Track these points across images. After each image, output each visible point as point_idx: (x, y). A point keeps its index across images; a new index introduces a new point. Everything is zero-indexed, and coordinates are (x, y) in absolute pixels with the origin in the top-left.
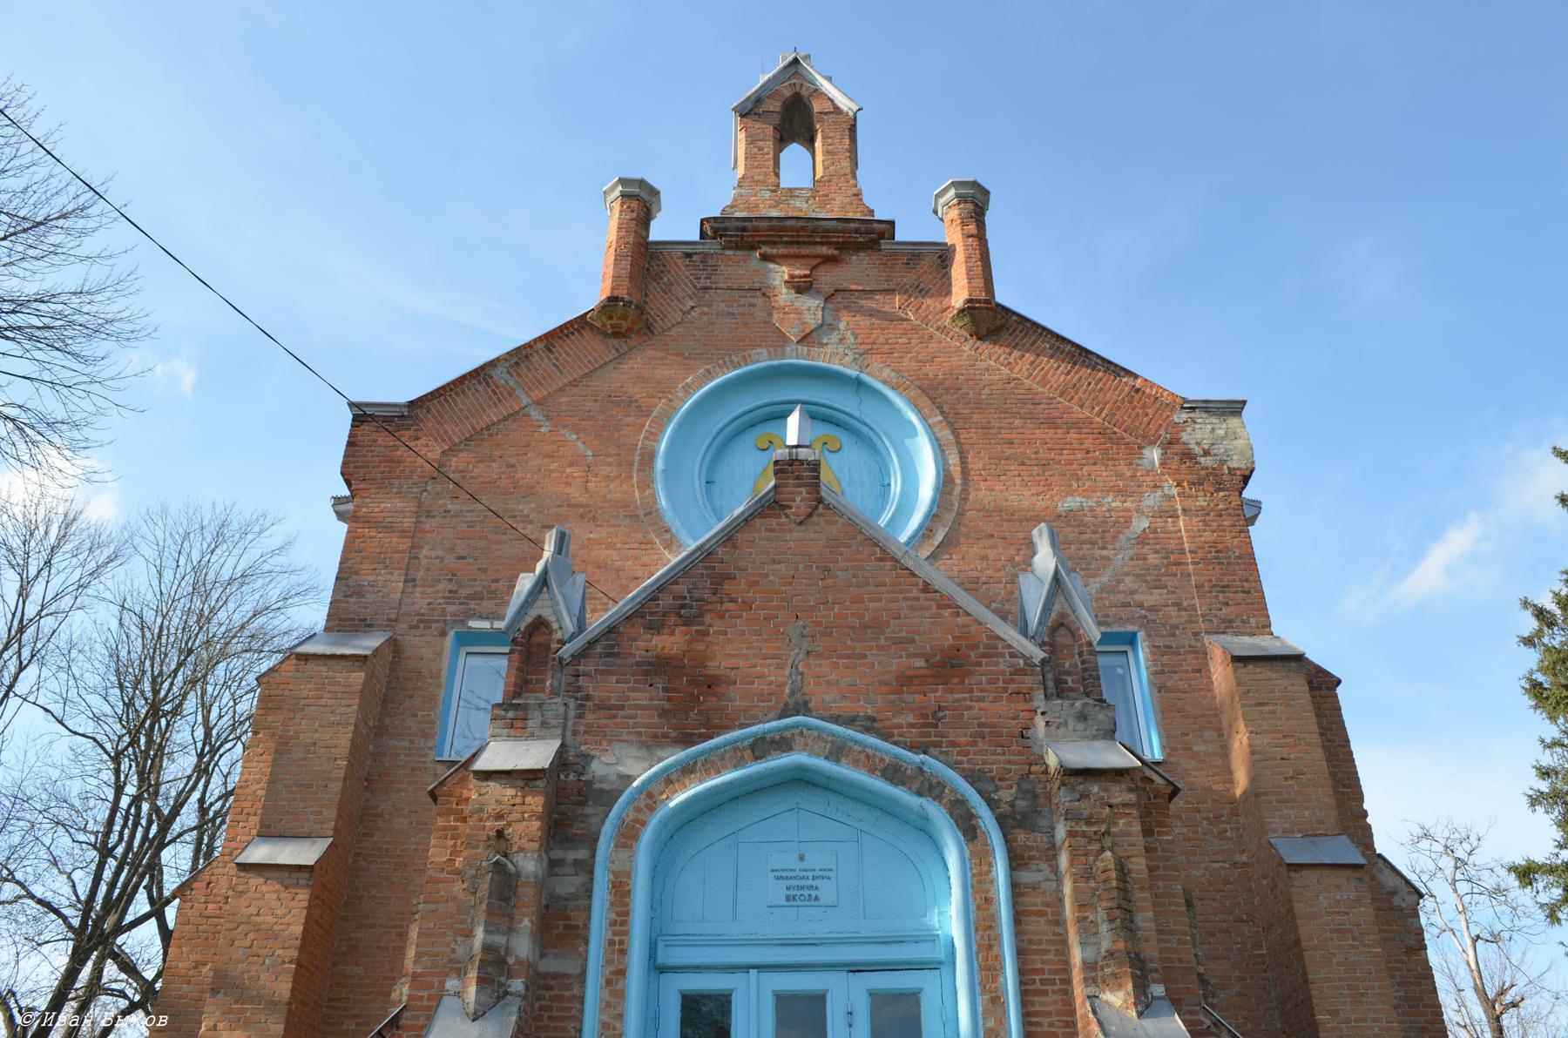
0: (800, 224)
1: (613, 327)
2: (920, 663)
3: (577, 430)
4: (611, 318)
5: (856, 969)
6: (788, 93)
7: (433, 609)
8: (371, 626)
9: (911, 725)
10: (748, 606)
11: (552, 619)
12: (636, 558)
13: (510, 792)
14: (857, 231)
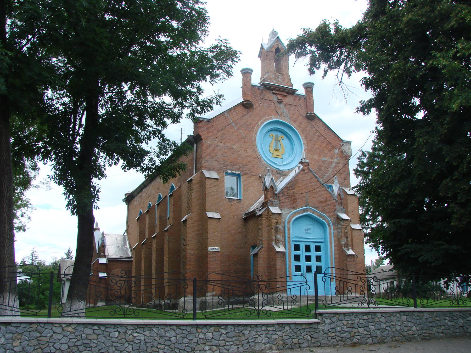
6: (276, 47)
8: (210, 169)
11: (273, 186)
14: (292, 91)
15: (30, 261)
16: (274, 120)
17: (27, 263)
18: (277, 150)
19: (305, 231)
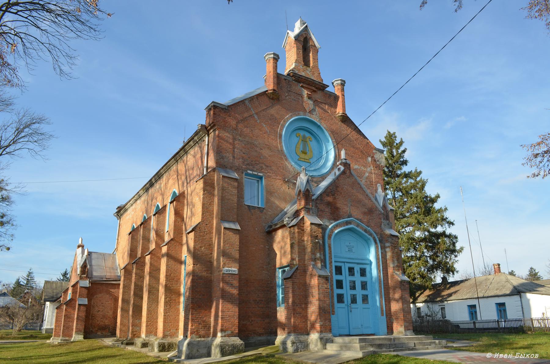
0: (311, 80)
1: (272, 97)
2: (366, 210)
3: (265, 124)
4: (273, 95)
5: (358, 264)
7: (239, 166)
9: (366, 222)
10: (341, 193)
11: (310, 190)
12: (279, 161)
13: (316, 228)
14: (322, 86)
15: (25, 282)
16: (302, 117)
17: (22, 283)
18: (304, 152)
19: (347, 250)
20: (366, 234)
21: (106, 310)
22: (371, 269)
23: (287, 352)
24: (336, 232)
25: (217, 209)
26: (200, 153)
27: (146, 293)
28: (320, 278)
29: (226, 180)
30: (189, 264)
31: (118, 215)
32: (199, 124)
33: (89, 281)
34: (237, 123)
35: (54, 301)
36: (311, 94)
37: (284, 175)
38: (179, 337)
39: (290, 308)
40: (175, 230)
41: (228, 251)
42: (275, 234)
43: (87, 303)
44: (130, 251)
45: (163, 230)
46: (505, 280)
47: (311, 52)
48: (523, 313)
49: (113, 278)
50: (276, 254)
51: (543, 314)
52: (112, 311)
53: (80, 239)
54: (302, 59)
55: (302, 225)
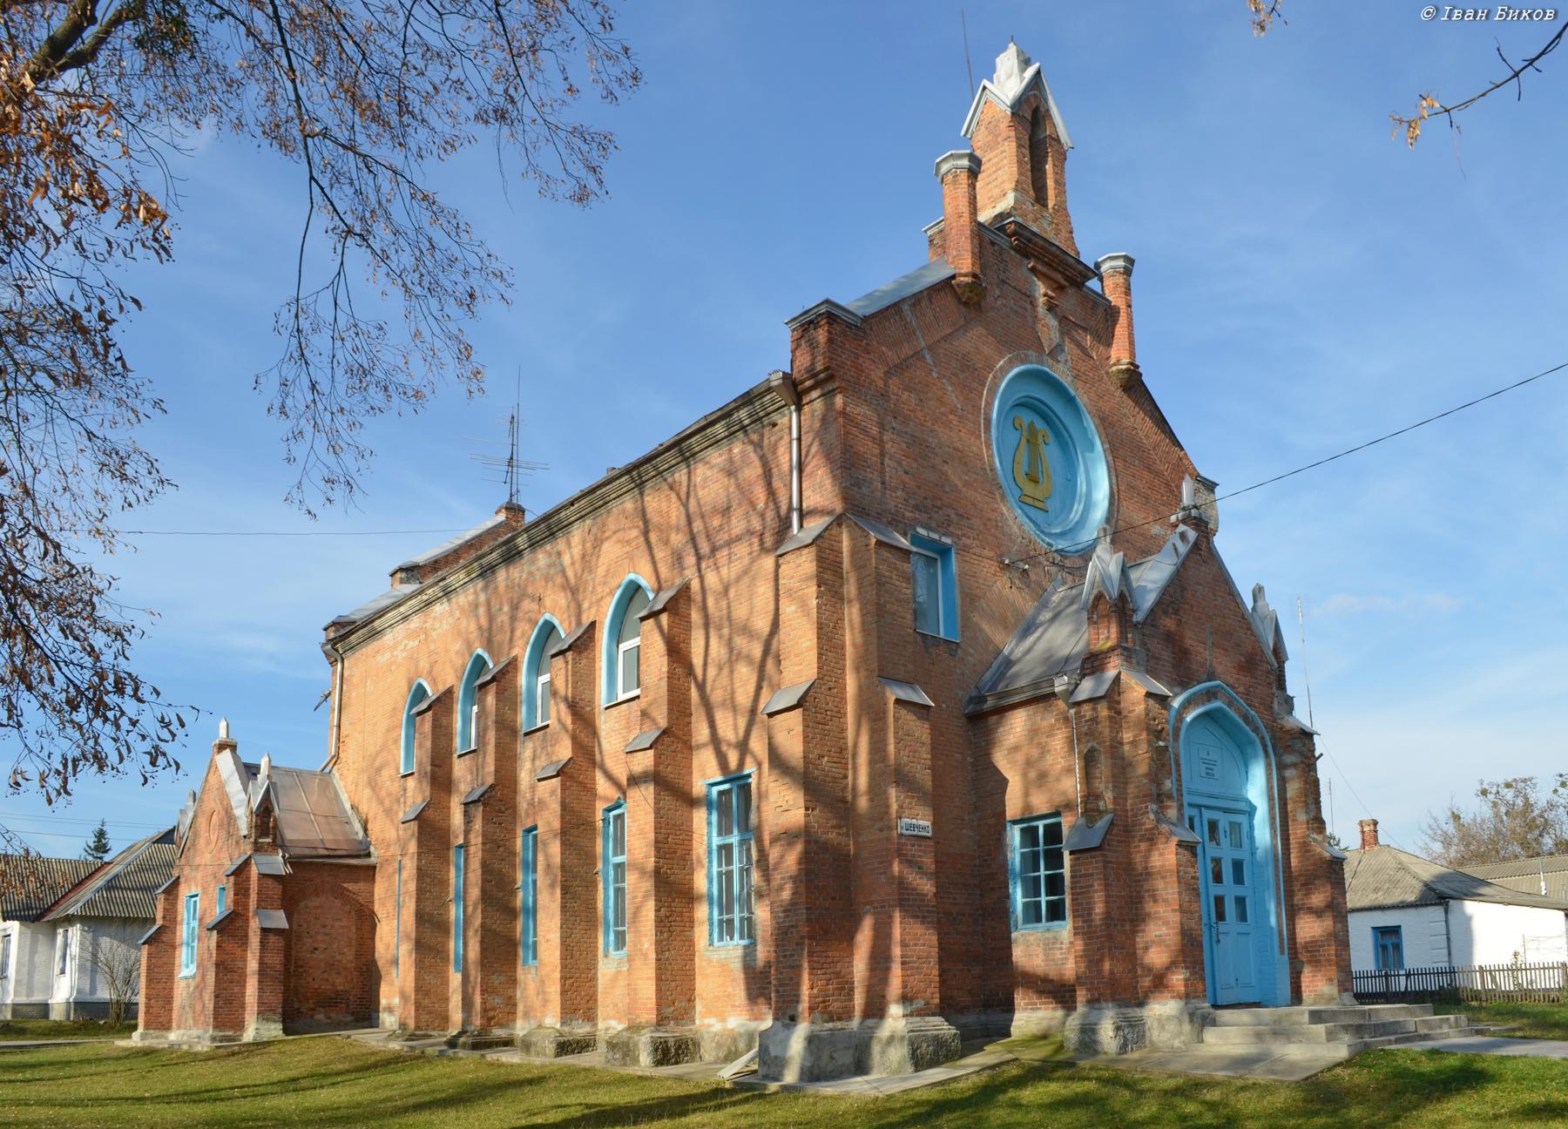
1: (969, 298)
3: (952, 384)
10: (1192, 606)
12: (987, 503)
20: (1247, 728)
21: (335, 946)
22: (1251, 827)
23: (1096, 1053)
24: (1189, 719)
25: (859, 640)
26: (757, 463)
27: (552, 894)
28: (1180, 850)
29: (885, 554)
30: (785, 808)
31: (337, 650)
32: (776, 372)
33: (283, 857)
34: (886, 373)
35: (37, 919)
36: (1053, 295)
37: (999, 546)
38: (697, 1022)
39: (1095, 932)
40: (671, 703)
41: (906, 769)
42: (999, 724)
43: (284, 924)
44: (432, 765)
45: (591, 702)
46: (1394, 865)
47: (1050, 159)
48: (1450, 954)
49: (344, 848)
50: (1004, 782)
51: (1516, 955)
52: (353, 949)
53: (223, 724)
54: (1030, 181)
55: (1117, 698)
